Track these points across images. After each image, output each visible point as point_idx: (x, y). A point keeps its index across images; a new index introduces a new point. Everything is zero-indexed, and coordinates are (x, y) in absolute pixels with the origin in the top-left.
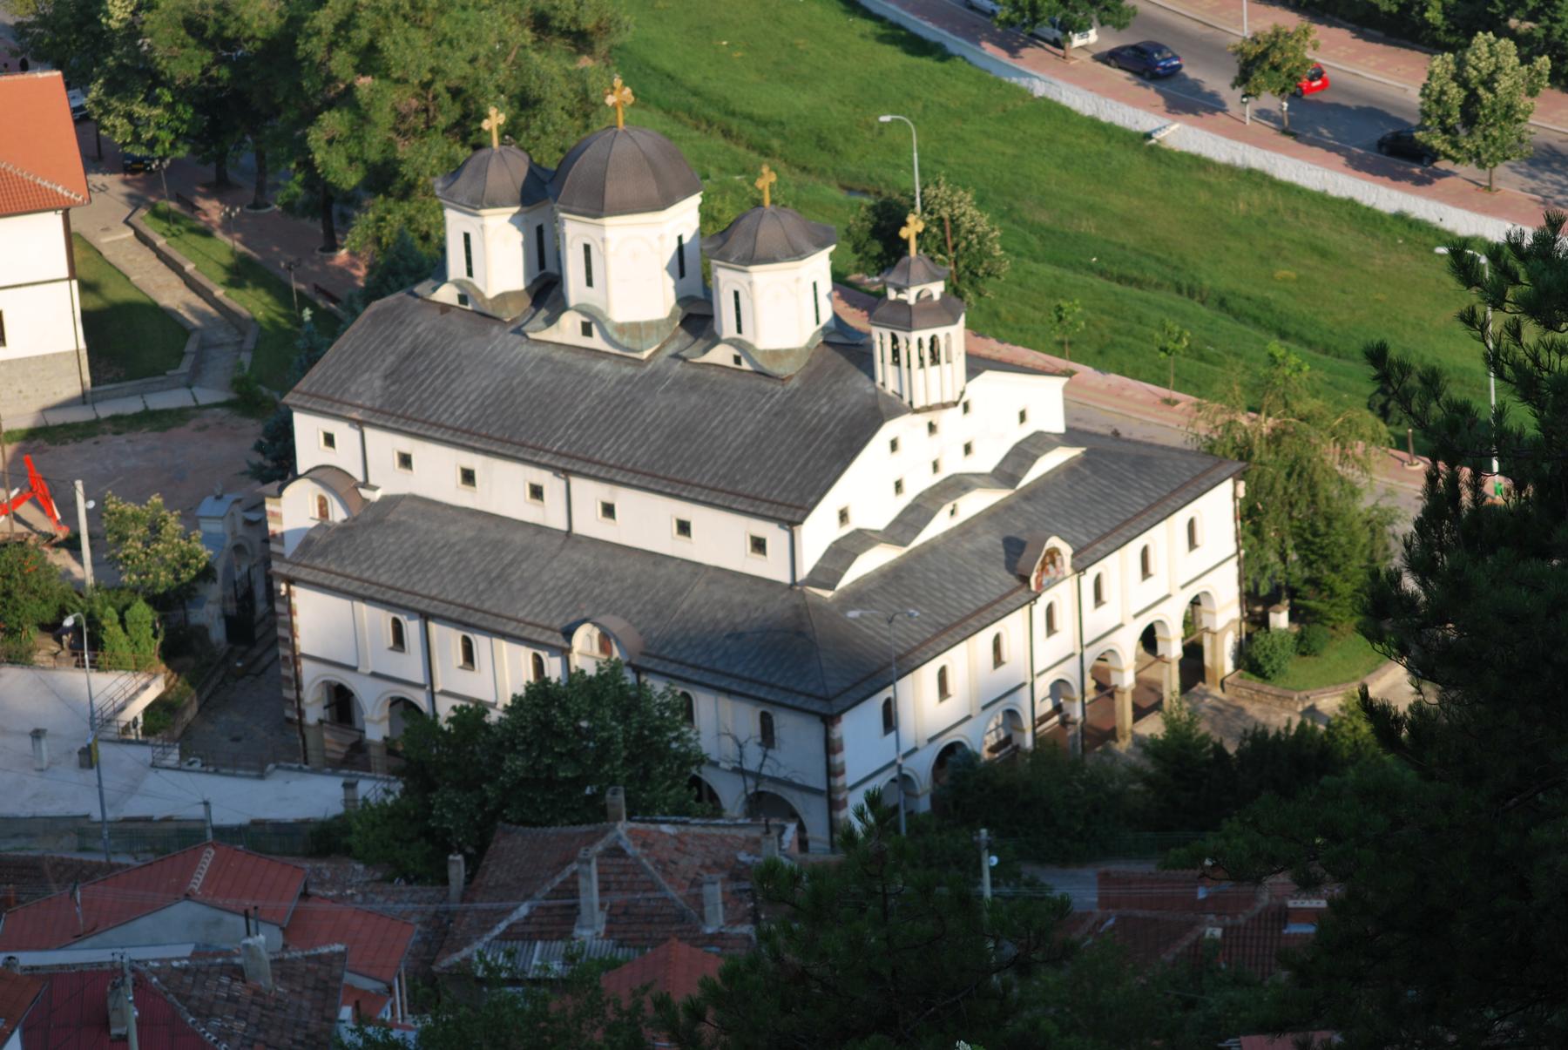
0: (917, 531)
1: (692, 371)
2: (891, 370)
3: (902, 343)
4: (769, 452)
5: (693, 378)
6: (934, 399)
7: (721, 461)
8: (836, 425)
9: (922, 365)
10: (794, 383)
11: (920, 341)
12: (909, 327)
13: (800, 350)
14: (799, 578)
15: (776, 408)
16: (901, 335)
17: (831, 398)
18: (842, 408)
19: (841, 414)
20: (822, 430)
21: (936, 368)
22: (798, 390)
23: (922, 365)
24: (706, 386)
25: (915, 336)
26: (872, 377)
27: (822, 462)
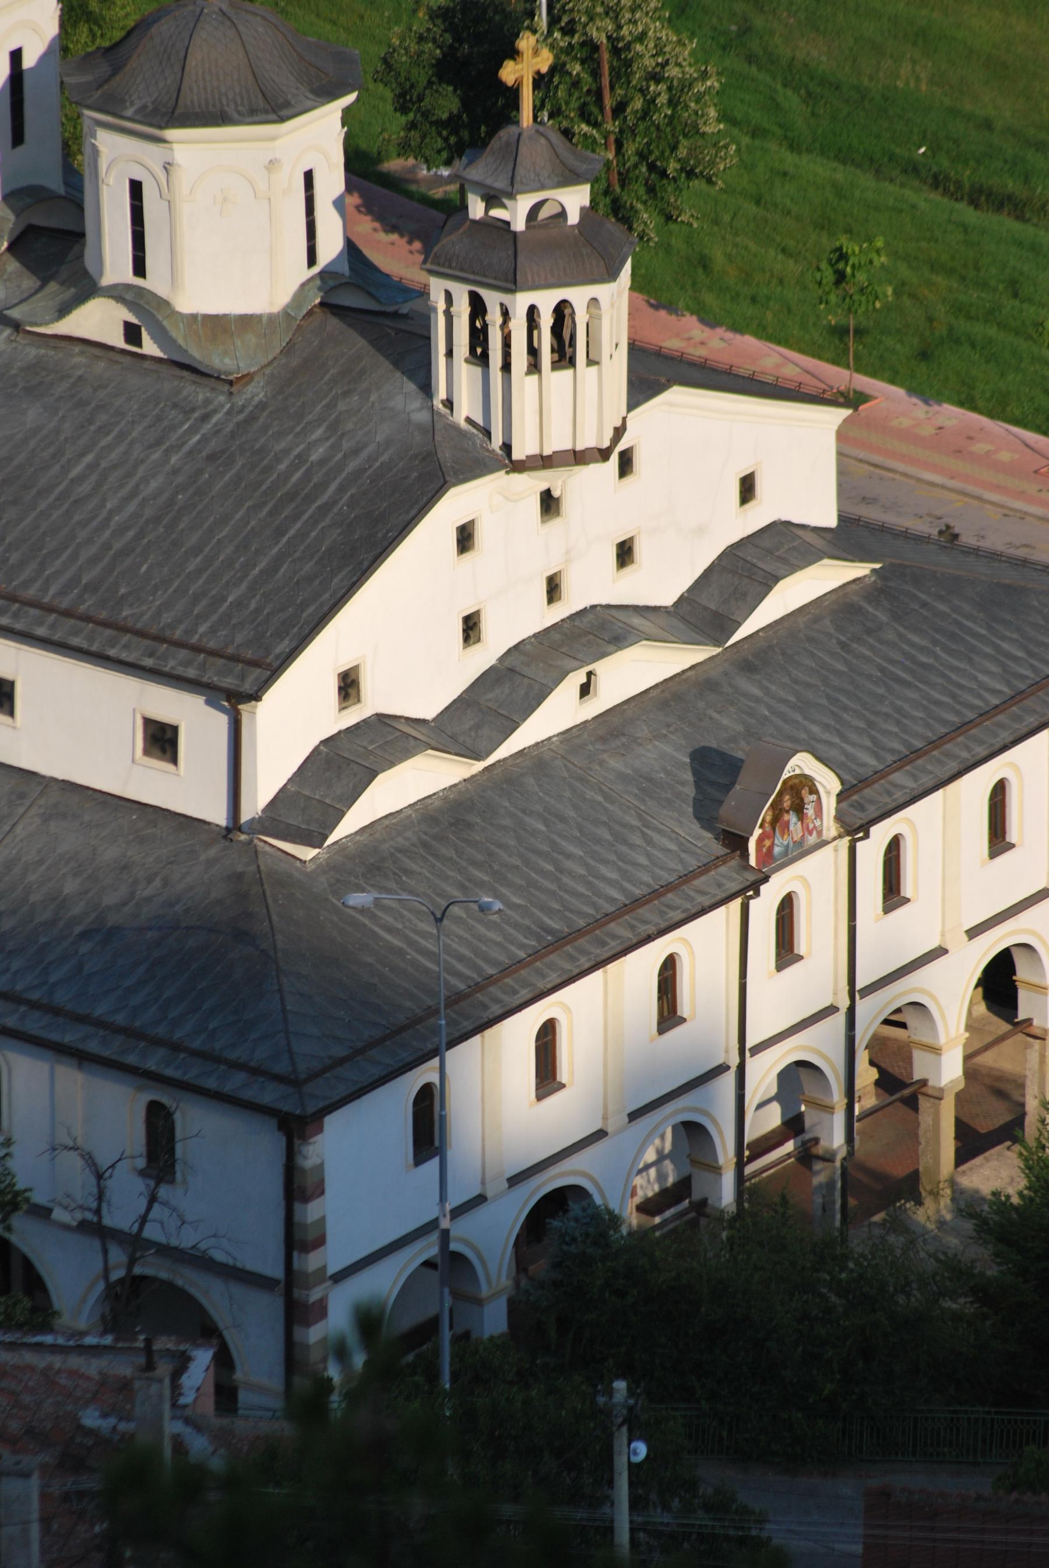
0: (512, 726)
1: (32, 352)
2: (466, 374)
3: (494, 317)
4: (194, 539)
5: (34, 367)
6: (558, 442)
7: (85, 555)
8: (342, 489)
9: (534, 367)
10: (256, 392)
11: (532, 312)
12: (511, 284)
13: (272, 318)
14: (245, 816)
15: (213, 445)
16: (492, 299)
17: (333, 428)
18: (356, 452)
19: (352, 465)
20: (310, 498)
21: (567, 374)
22: (262, 406)
23: (534, 367)
24: (61, 388)
25: (521, 302)
26: (427, 388)
27: (308, 567)
